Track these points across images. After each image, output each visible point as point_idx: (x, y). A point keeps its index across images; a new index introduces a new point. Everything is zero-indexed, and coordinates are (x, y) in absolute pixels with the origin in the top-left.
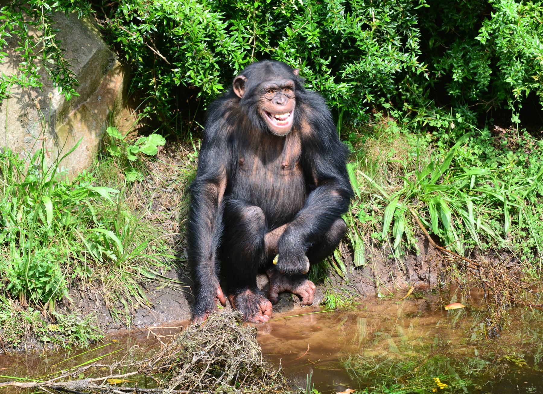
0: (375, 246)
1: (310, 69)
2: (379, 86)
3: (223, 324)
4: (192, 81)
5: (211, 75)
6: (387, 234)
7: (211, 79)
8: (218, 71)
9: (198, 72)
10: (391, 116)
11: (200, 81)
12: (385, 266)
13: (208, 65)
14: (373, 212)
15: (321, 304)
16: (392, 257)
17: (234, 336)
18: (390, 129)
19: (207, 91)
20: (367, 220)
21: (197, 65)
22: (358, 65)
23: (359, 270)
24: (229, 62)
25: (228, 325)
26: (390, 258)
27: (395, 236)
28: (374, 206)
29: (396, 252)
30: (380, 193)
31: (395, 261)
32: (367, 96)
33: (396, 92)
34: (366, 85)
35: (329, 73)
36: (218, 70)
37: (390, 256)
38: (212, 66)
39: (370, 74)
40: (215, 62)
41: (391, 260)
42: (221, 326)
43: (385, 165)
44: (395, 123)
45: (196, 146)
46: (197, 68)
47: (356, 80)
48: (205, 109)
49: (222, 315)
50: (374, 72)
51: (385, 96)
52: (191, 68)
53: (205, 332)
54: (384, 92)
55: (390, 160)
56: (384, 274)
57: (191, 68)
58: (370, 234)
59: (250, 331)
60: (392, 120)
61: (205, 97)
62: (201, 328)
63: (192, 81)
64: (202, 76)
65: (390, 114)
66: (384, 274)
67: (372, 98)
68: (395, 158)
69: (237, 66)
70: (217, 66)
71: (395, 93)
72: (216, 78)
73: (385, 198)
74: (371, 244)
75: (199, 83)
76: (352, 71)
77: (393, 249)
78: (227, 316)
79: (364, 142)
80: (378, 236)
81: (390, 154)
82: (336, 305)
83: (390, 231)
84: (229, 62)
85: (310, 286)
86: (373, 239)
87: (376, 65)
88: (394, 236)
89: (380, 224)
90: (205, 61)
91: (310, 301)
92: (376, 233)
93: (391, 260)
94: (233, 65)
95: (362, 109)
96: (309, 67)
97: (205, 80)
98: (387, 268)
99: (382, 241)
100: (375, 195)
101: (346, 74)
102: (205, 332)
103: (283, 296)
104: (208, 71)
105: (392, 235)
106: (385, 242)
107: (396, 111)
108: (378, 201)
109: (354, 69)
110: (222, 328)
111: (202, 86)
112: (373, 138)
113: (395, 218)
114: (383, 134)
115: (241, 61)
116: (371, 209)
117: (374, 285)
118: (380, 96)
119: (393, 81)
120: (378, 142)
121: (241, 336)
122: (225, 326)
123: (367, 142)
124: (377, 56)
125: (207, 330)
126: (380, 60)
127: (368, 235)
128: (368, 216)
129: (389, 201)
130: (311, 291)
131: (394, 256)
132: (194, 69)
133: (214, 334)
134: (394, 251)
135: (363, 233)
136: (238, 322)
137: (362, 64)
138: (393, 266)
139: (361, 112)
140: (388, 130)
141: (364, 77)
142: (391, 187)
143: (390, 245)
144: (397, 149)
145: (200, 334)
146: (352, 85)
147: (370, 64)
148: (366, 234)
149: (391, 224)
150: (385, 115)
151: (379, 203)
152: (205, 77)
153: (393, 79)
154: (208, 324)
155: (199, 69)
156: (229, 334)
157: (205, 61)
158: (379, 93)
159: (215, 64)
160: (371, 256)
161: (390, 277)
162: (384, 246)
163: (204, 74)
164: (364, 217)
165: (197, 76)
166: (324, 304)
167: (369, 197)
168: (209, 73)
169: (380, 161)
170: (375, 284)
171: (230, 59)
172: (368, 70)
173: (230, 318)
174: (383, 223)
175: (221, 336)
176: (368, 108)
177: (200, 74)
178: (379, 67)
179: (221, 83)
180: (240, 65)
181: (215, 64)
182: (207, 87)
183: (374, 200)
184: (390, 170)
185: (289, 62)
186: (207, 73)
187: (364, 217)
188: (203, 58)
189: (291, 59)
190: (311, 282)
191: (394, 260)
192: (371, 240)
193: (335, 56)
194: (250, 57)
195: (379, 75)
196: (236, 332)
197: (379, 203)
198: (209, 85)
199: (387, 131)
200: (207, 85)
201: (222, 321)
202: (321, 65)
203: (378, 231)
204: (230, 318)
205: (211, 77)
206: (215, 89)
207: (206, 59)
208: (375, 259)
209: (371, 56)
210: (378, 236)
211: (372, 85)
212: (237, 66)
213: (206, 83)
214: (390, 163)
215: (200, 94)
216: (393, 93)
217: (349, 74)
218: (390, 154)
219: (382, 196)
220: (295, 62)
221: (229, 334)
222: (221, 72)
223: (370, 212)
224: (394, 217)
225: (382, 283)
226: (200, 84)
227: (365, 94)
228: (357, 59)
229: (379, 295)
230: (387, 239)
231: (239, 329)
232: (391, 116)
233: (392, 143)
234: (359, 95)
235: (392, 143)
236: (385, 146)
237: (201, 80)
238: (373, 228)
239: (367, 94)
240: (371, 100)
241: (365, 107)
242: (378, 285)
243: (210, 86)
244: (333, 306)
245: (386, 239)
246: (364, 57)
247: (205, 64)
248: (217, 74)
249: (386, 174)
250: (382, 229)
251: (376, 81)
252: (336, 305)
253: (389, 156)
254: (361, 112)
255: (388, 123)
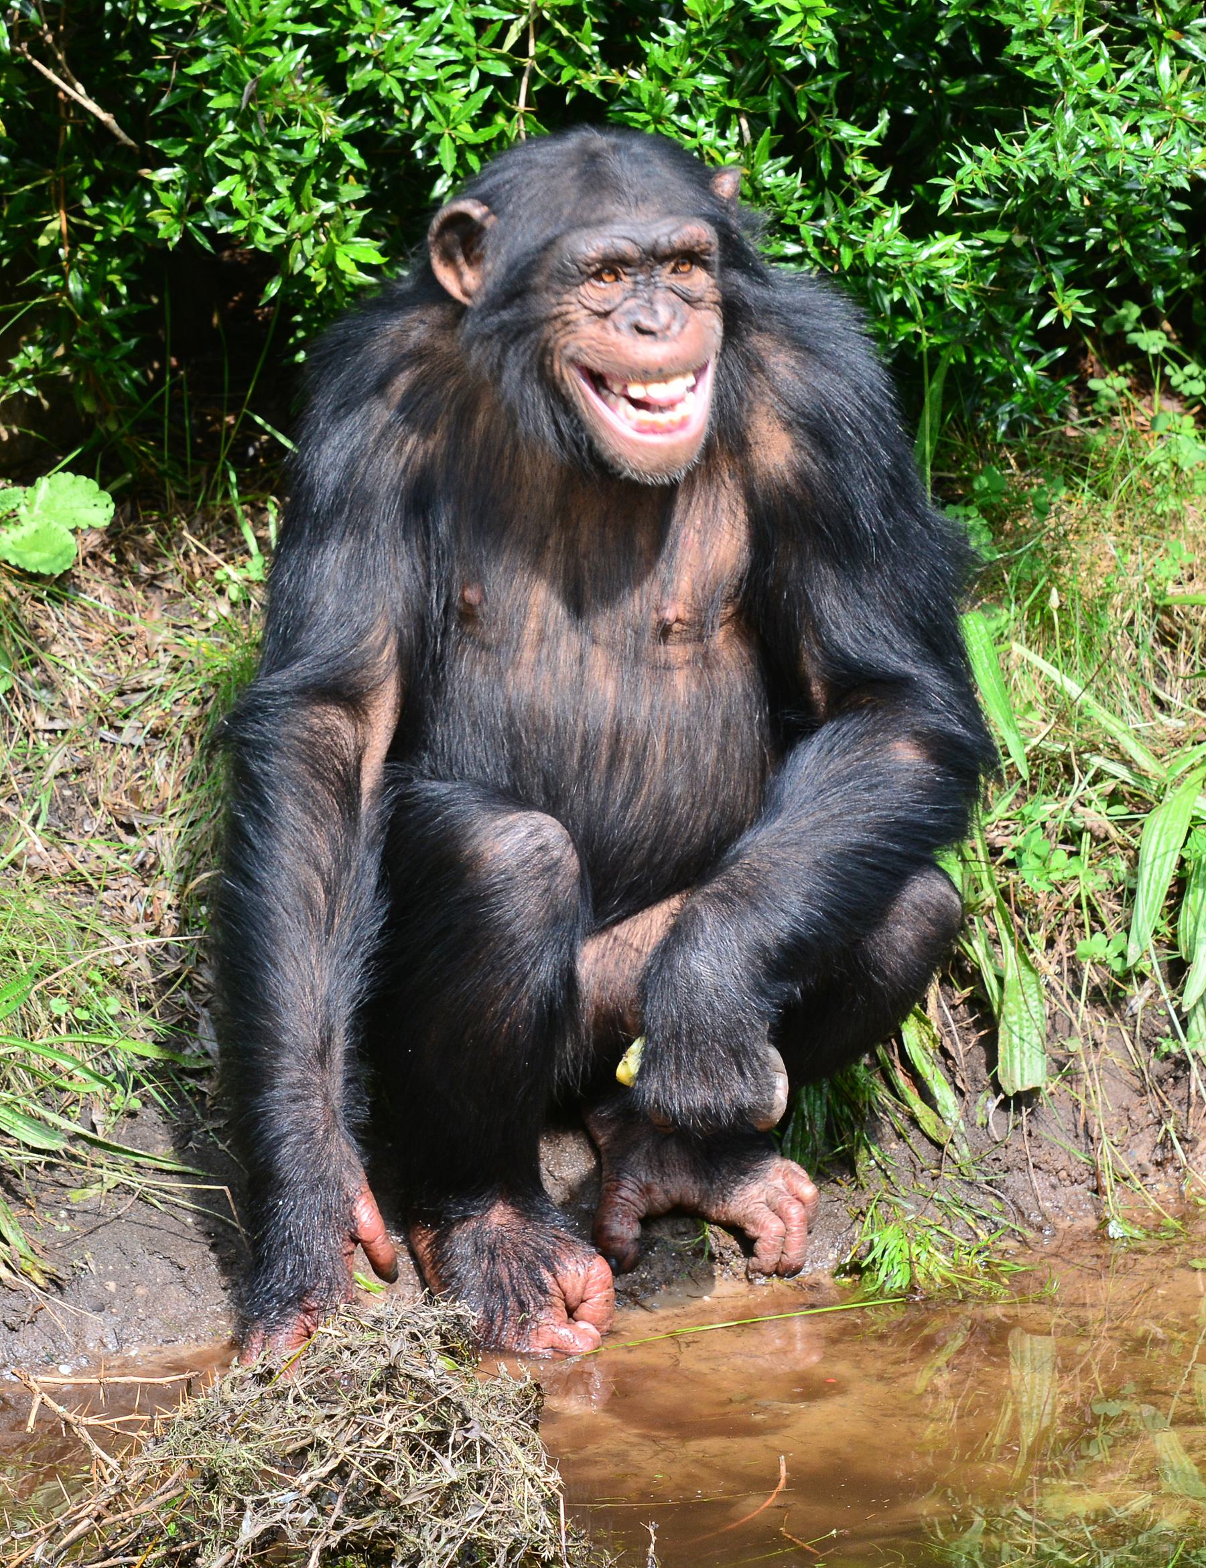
0: (1096, 997)
1: (789, 170)
2: (1113, 247)
3: (383, 1362)
4: (240, 225)
5: (328, 196)
6: (1150, 942)
7: (325, 217)
8: (360, 181)
9: (267, 181)
10: (1171, 392)
11: (276, 228)
12: (1142, 1093)
13: (312, 150)
14: (1086, 837)
15: (842, 1270)
16: (1175, 1050)
17: (436, 1419)
18: (1167, 448)
19: (309, 272)
20: (1056, 877)
21: (262, 150)
22: (1016, 150)
23: (1018, 1110)
24: (409, 138)
25: (405, 1368)
26: (1167, 1056)
27: (1191, 952)
28: (1090, 810)
29: (1193, 1026)
30: (1116, 749)
31: (1188, 1067)
32: (1057, 295)
33: (1191, 276)
34: (1051, 243)
35: (880, 186)
36: (359, 175)
37: (1167, 1045)
38: (332, 154)
39: (1073, 194)
40: (346, 138)
41: (1169, 1066)
42: (375, 1375)
43: (1141, 617)
44: (1189, 420)
45: (255, 529)
46: (261, 167)
47: (1008, 221)
48: (301, 357)
49: (378, 1321)
50: (1092, 184)
51: (1141, 296)
52: (234, 164)
53: (297, 1400)
54: (1136, 277)
55: (1163, 595)
56: (1136, 1129)
57: (234, 164)
58: (1072, 944)
59: (511, 1396)
60: (1172, 408)
61: (300, 300)
62: (280, 1382)
63: (240, 225)
64: (284, 204)
65: (1166, 379)
66: (1136, 1129)
67: (1079, 307)
68: (1188, 587)
69: (446, 157)
70: (353, 157)
71: (1188, 280)
72: (348, 213)
73: (1141, 776)
74: (1077, 991)
75: (269, 233)
76: (987, 180)
77: (1178, 1010)
78: (402, 1324)
79: (1042, 512)
80: (1111, 953)
81: (1167, 569)
82: (913, 1277)
83: (1167, 930)
84: (409, 138)
85: (790, 1187)
86: (1087, 966)
87: (1098, 152)
88: (1182, 953)
89: (1119, 896)
90: (296, 132)
91: (792, 1257)
92: (1099, 936)
93: (1169, 1066)
94: (431, 151)
95: (1033, 357)
96: (784, 160)
97: (297, 221)
98: (1152, 1100)
99: (1126, 977)
100: (1097, 762)
101: (961, 193)
102: (297, 1400)
103: (662, 1233)
104: (312, 179)
105: (1173, 946)
106: (1142, 977)
107: (1192, 368)
108: (1108, 786)
109: (997, 171)
110: (376, 1384)
111: (283, 250)
112: (1087, 495)
113: (1189, 866)
114: (1134, 473)
115: (466, 131)
116: (1077, 823)
117: (1091, 1183)
118: (1118, 297)
119: (1177, 227)
120: (1109, 510)
121: (467, 1419)
122: (391, 1371)
123: (1059, 511)
124: (1104, 111)
125: (309, 1392)
126: (1117, 129)
127: (1061, 946)
128: (1060, 857)
129: (1163, 790)
130: (795, 1211)
131: (1186, 1046)
132: (246, 167)
133: (339, 1411)
134: (1185, 1024)
135: (1038, 939)
136: (452, 1352)
137: (1033, 146)
138: (1181, 1093)
139: (1028, 369)
140: (1155, 454)
141: (1045, 206)
142: (1172, 723)
143: (1166, 994)
144: (1197, 543)
145: (276, 1412)
146: (988, 245)
147: (1070, 148)
148: (1051, 943)
149: (1169, 896)
150: (1143, 385)
151: (1114, 798)
152: (299, 209)
153: (1178, 216)
154: (312, 1361)
155: (272, 168)
156: (411, 1409)
157: (296, 132)
158: (1112, 283)
159: (345, 147)
160: (1074, 1045)
161: (1164, 1144)
162: (1138, 997)
163: (295, 191)
164: (1044, 861)
165: (263, 203)
166: (855, 1269)
167: (1068, 769)
168: (316, 187)
169: (1117, 600)
170: (1096, 1174)
171: (416, 120)
172: (1061, 175)
173: (414, 1337)
174: (1132, 892)
175: (373, 1419)
176: (1061, 352)
177: (278, 195)
178: (1111, 160)
179: (375, 237)
180: (460, 152)
181: (345, 147)
182: (309, 252)
183: (1092, 783)
184: (1164, 642)
185: (693, 135)
186: (308, 189)
187: (1044, 861)
188: (291, 117)
189: (702, 121)
190: (794, 1166)
191: (1182, 1064)
192: (1075, 972)
193: (909, 111)
194: (510, 115)
195: (1112, 198)
196: (446, 1401)
197: (1114, 798)
198: (317, 243)
199: (1150, 459)
200: (308, 244)
201: (379, 1348)
202: (840, 151)
203: (1109, 927)
204: (414, 1337)
205: (328, 207)
206: (343, 263)
207: (305, 123)
208: (1094, 1061)
209: (1075, 107)
210: (1111, 953)
211: (1082, 243)
212: (446, 157)
213: (305, 235)
214: (1167, 611)
215: (273, 289)
216: (1178, 280)
217: (975, 193)
218: (1167, 569)
219: (1128, 763)
220: (722, 135)
221: (411, 1409)
222: (374, 184)
223: (1071, 837)
224: (1182, 862)
225: (1128, 1171)
226: (276, 241)
227: (1050, 286)
228: (1010, 124)
229: (1115, 1230)
230: (1153, 966)
231: (456, 1389)
232: (1171, 392)
233: (1177, 517)
234: (1019, 293)
235: (1177, 517)
236: (1139, 531)
237: (281, 219)
238: (1085, 916)
239: (1058, 285)
240: (1076, 315)
241: (1050, 347)
242: (1107, 1181)
243: (322, 249)
244: (900, 1280)
245: (1144, 966)
246: (1042, 113)
247: (298, 145)
248: (353, 191)
249: (1145, 662)
250: (1128, 920)
251: (1098, 224)
252: (913, 1277)
253: (1160, 577)
254: (1028, 369)
255: (1154, 421)
